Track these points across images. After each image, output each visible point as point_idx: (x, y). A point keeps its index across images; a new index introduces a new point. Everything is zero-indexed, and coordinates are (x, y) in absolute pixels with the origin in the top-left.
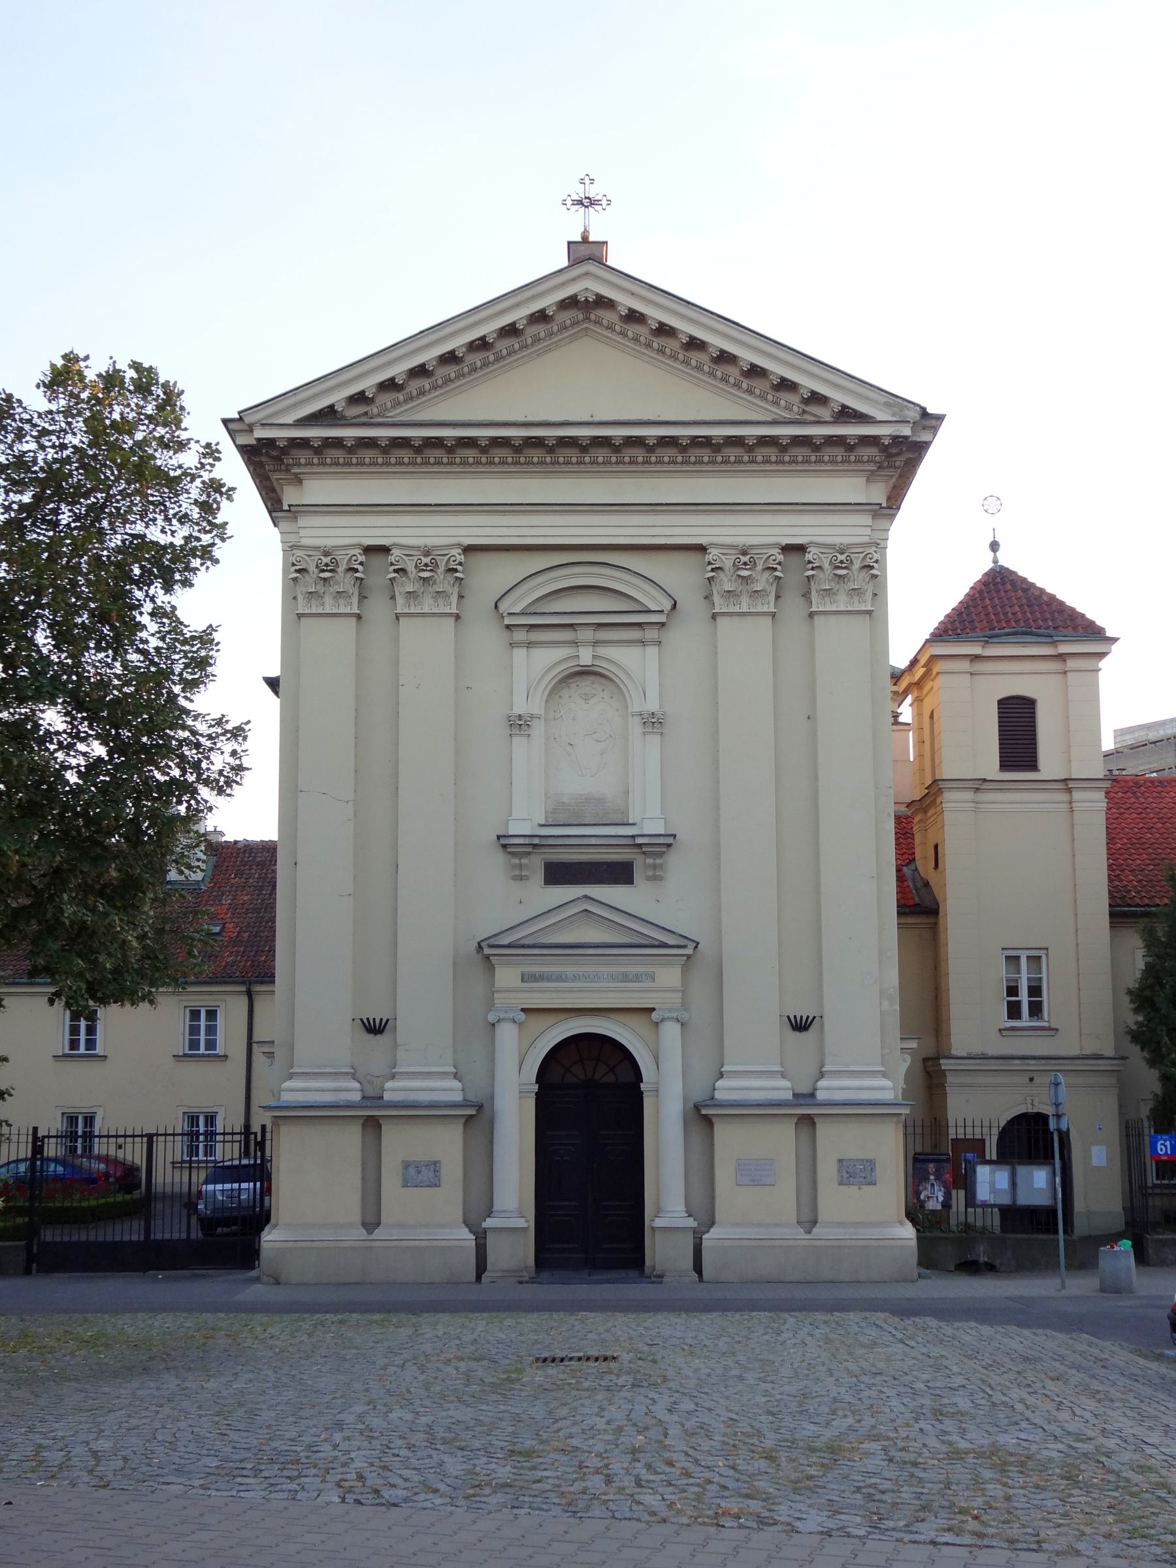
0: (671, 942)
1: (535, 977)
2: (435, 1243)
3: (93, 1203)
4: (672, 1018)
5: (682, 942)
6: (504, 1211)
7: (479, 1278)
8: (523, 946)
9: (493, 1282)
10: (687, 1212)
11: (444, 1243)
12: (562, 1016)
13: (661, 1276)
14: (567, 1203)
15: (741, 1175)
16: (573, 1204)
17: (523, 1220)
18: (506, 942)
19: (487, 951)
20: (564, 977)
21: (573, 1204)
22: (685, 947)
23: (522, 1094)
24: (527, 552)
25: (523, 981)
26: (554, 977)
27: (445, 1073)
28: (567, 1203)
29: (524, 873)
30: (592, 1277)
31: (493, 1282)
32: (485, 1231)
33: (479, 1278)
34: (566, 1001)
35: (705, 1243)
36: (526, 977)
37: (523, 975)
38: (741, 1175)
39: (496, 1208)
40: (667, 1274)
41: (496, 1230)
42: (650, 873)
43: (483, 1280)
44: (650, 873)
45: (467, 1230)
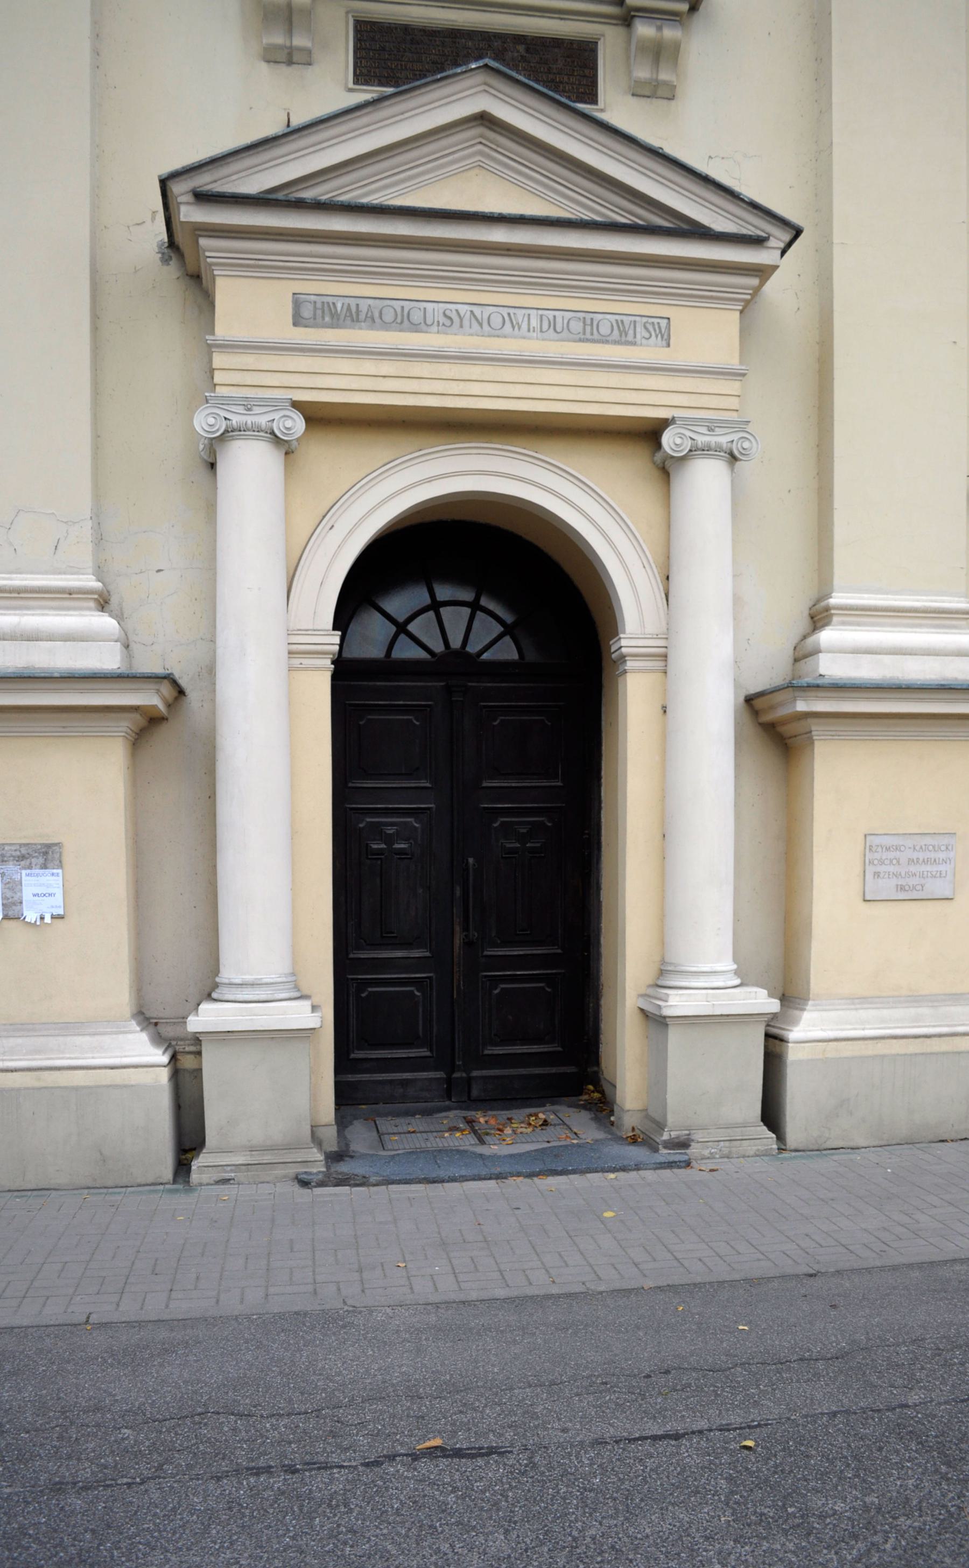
0: (720, 224)
1: (334, 315)
2: (50, 1079)
3: (560, 931)
4: (718, 448)
5: (753, 225)
6: (253, 985)
7: (182, 1167)
8: (299, 205)
9: (226, 1181)
10: (737, 973)
11: (79, 1079)
12: (404, 443)
13: (683, 1144)
14: (399, 954)
15: (877, 875)
16: (416, 953)
17: (306, 1004)
18: (253, 185)
19: (190, 214)
20: (417, 317)
21: (416, 953)
22: (757, 241)
23: (296, 662)
24: (250, 195)
25: (298, 321)
26: (388, 316)
27: (70, 593)
28: (399, 954)
29: (299, 41)
30: (494, 1148)
31: (226, 1181)
32: (197, 1039)
33: (182, 1167)
34: (426, 386)
35: (794, 1055)
36: (307, 312)
37: (297, 303)
38: (877, 875)
39: (227, 974)
40: (698, 1136)
41: (227, 1037)
42: (643, 73)
43: (195, 1177)
44: (643, 73)
45: (144, 1037)
